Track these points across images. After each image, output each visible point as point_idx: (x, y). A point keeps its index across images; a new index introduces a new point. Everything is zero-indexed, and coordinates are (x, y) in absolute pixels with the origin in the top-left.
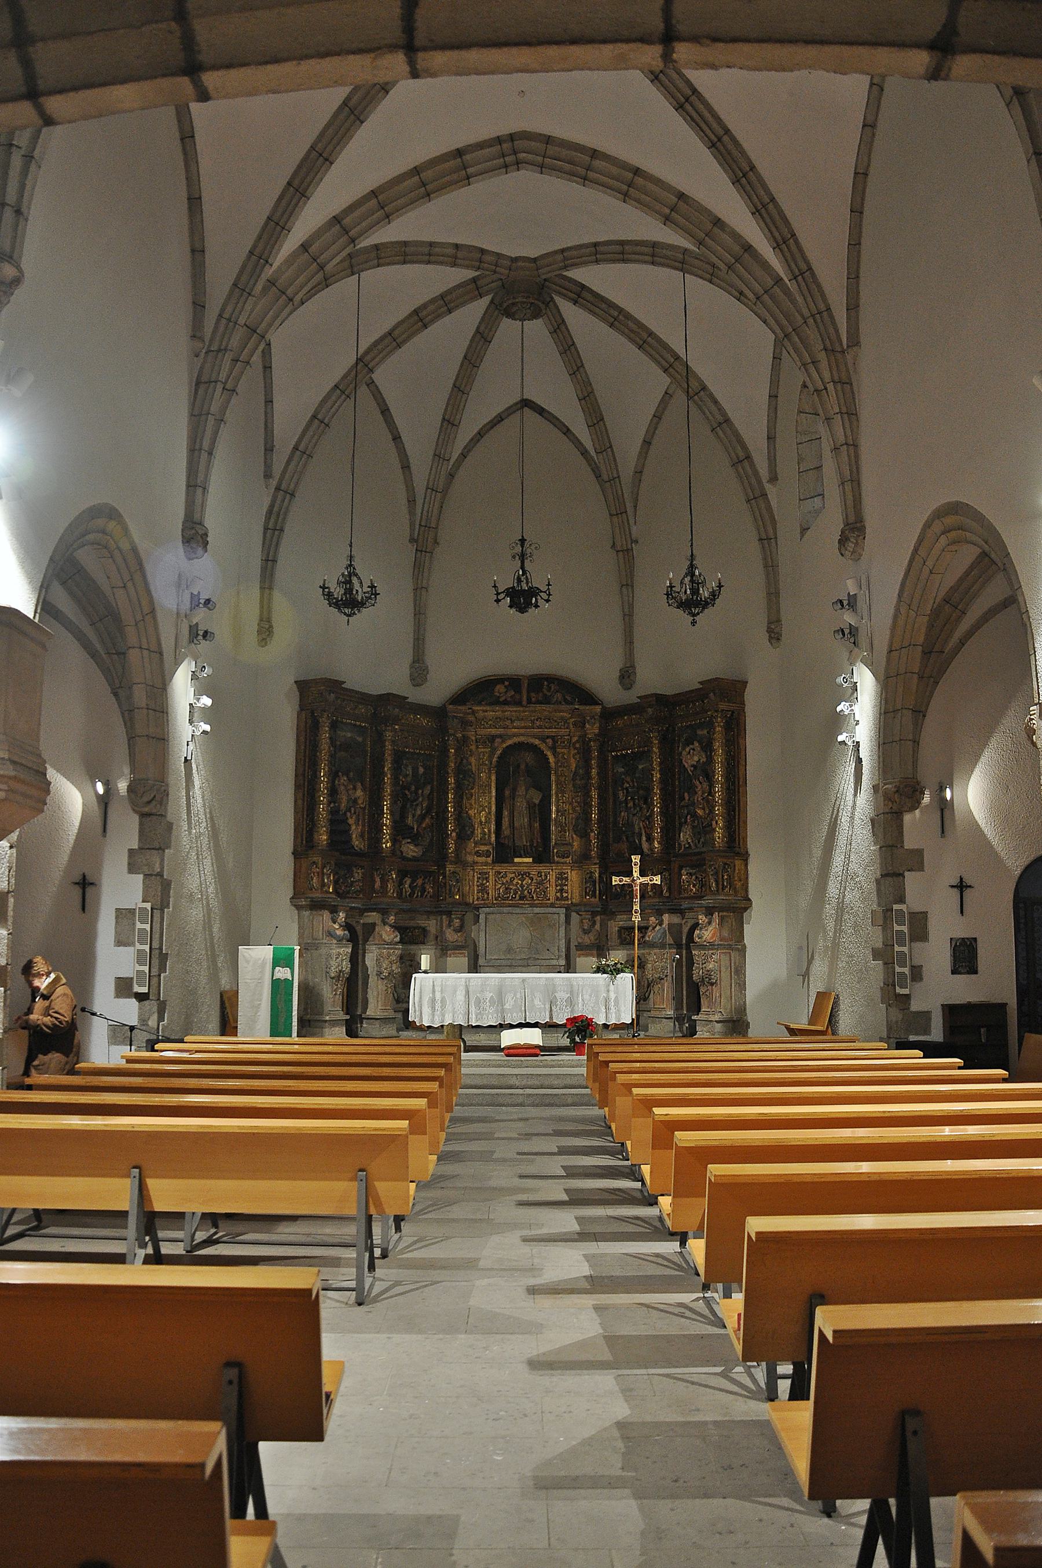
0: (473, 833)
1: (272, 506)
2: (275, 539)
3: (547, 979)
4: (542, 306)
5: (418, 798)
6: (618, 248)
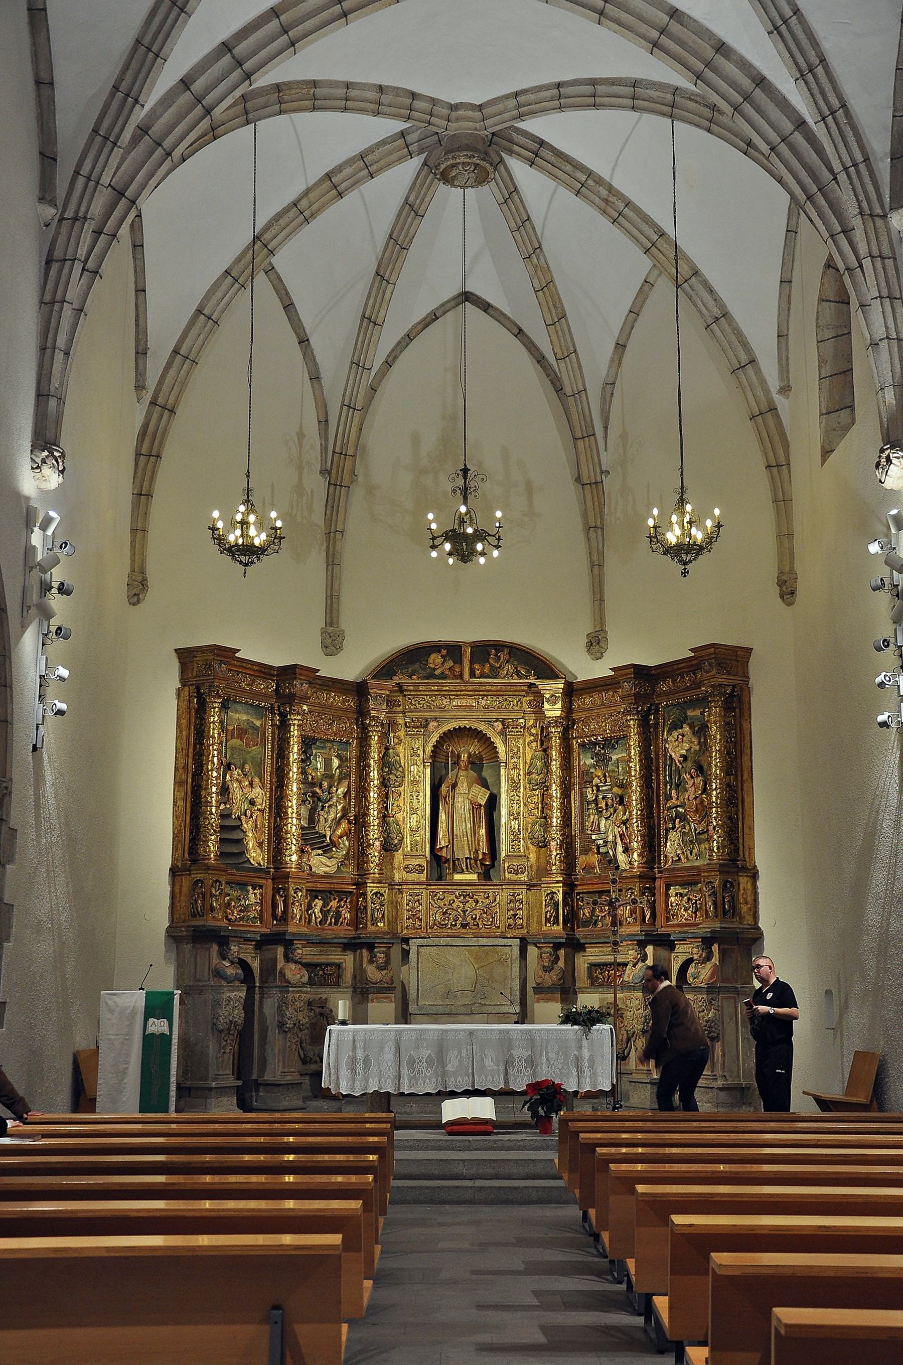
0: (401, 841)
1: (145, 426)
2: (150, 467)
3: (501, 1031)
4: (491, 169)
5: (331, 798)
6: (588, 89)
